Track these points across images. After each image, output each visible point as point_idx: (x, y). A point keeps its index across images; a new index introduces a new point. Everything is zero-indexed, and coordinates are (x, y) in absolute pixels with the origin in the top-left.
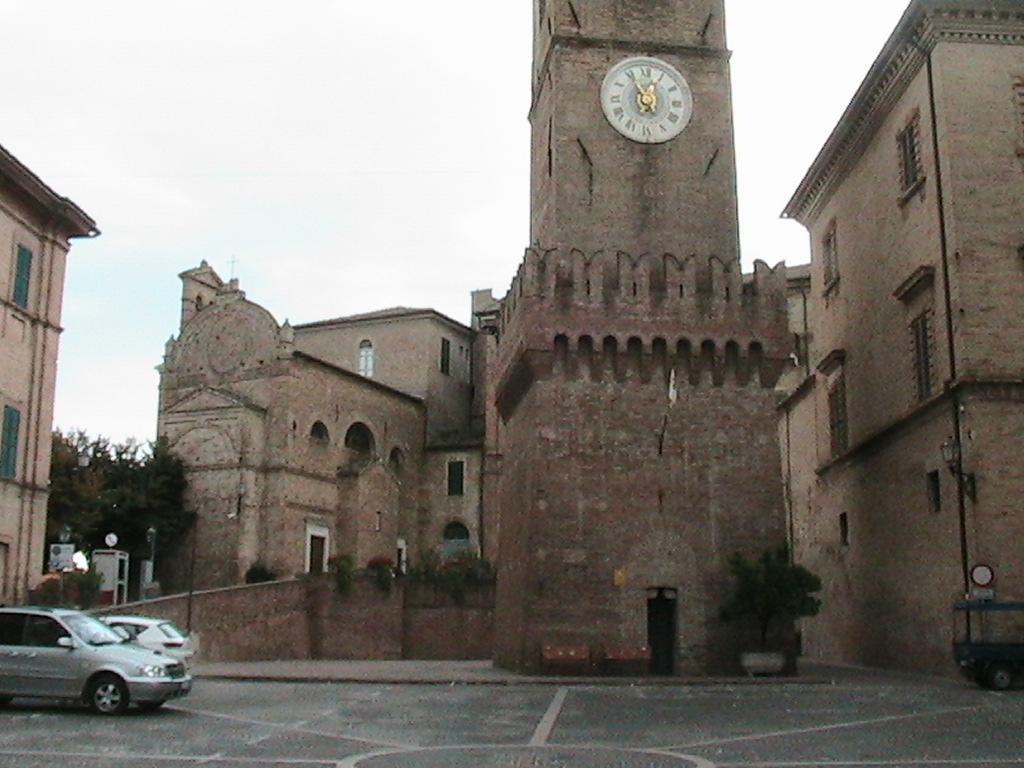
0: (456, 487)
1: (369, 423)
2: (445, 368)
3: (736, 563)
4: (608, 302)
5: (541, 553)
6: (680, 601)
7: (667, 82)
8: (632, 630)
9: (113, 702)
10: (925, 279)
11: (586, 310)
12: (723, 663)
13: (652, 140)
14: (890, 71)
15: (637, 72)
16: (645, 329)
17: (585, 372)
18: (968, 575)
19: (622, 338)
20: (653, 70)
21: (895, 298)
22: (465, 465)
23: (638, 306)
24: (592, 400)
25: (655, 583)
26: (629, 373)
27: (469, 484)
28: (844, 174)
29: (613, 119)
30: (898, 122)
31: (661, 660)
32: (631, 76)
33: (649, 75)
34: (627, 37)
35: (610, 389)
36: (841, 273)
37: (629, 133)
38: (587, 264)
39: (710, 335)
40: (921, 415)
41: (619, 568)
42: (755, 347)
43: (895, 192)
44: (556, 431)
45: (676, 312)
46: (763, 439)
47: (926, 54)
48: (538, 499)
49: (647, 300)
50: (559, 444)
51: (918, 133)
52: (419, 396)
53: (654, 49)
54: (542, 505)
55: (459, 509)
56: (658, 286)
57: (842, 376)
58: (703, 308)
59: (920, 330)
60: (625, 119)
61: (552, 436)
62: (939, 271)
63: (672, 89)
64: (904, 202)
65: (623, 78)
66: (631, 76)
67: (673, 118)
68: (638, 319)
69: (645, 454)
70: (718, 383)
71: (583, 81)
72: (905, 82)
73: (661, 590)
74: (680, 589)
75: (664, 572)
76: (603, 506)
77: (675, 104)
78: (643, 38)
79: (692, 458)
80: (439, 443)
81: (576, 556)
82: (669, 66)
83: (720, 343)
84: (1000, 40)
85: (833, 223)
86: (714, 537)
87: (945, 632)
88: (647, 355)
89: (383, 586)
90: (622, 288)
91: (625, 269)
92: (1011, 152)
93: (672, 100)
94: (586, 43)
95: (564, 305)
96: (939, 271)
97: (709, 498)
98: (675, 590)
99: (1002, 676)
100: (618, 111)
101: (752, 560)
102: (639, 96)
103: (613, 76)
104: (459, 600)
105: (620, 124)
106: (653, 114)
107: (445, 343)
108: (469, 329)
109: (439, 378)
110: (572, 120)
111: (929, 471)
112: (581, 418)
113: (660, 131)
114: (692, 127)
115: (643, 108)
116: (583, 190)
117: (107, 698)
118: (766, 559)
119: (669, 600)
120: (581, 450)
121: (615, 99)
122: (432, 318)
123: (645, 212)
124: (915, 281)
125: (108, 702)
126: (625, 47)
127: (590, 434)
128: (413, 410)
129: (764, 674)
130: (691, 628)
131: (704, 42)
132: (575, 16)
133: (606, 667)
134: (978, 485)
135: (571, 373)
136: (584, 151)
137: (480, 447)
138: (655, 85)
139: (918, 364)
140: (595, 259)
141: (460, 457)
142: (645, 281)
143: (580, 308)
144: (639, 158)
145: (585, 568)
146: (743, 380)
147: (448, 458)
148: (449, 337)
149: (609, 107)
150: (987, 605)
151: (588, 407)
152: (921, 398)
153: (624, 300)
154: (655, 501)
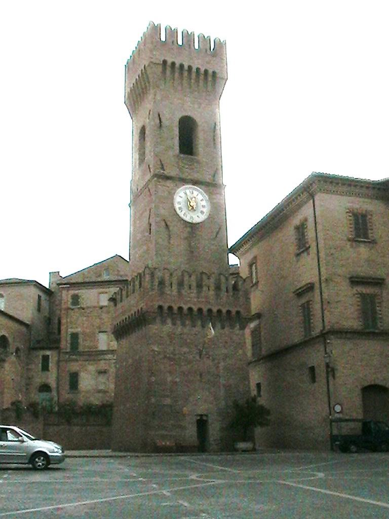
0: (45, 368)
1: (7, 335)
2: (39, 310)
3: (236, 405)
4: (179, 292)
5: (153, 400)
6: (210, 421)
7: (200, 197)
8: (191, 433)
9: (43, 464)
10: (310, 288)
11: (170, 295)
12: (228, 447)
13: (194, 222)
14: (293, 200)
15: (188, 191)
16: (195, 304)
17: (169, 321)
18: (331, 409)
19: (185, 307)
20: (194, 191)
21: (294, 294)
22: (50, 357)
23: (192, 294)
24: (172, 334)
25: (199, 413)
26: (187, 322)
27: (52, 365)
28: (262, 238)
29: (178, 211)
30: (296, 221)
31: (201, 447)
32: (186, 194)
33: (193, 193)
34: (183, 176)
35: (179, 330)
36: (260, 280)
37: (185, 218)
38: (171, 275)
39: (220, 307)
40: (305, 344)
41: (185, 406)
42: (238, 313)
43: (293, 249)
44: (158, 347)
45: (206, 297)
46: (240, 352)
47: (312, 196)
48: (150, 376)
49: (195, 291)
50: (159, 353)
51: (307, 227)
52: (28, 323)
53: (195, 183)
54: (153, 379)
55: (47, 378)
56: (199, 286)
57: (259, 324)
58: (218, 296)
59: (306, 309)
60: (183, 213)
61: (156, 349)
62: (317, 285)
63: (202, 200)
64: (298, 255)
65: (182, 194)
66: (186, 194)
67: (202, 212)
68: (191, 300)
69: (194, 357)
70: (223, 328)
71: (166, 194)
72: (300, 206)
73: (201, 415)
74: (209, 415)
75: (202, 409)
76: (178, 380)
77: (203, 206)
78: (189, 177)
79: (213, 360)
80: (37, 346)
81: (168, 401)
82: (201, 190)
83: (224, 311)
84: (342, 194)
85: (255, 258)
86: (222, 392)
87: (322, 433)
88: (195, 315)
89: (35, 415)
90: (185, 286)
91: (186, 278)
92: (345, 238)
93: (202, 204)
94: (168, 178)
95: (162, 293)
96: (317, 285)
97: (220, 377)
98: (206, 416)
99: (353, 448)
100: (180, 208)
101: (241, 402)
102: (189, 203)
103: (179, 193)
104: (69, 422)
105: (181, 215)
106: (195, 210)
107: (39, 297)
108: (47, 289)
109: (36, 313)
110: (162, 211)
111: (310, 366)
112: (168, 343)
113: (197, 218)
114: (210, 217)
115: (191, 208)
116: (166, 243)
117: (40, 463)
118: (247, 402)
119: (204, 420)
120: (168, 355)
121: (179, 203)
122: (35, 285)
123: (192, 252)
124: (305, 288)
125: (41, 464)
126: (184, 181)
127: (172, 349)
128: (24, 329)
129: (244, 451)
130: (215, 430)
131: (214, 181)
132: (162, 165)
133: (181, 449)
134: (336, 372)
135: (164, 322)
136: (167, 225)
137: (58, 348)
138: (195, 198)
139: (304, 322)
140: (175, 273)
141: (48, 353)
142: (194, 284)
143: (168, 295)
144: (189, 229)
145: (171, 406)
146: (232, 326)
147: (42, 353)
148: (41, 294)
149: (177, 206)
150: (341, 420)
151: (171, 336)
152: (305, 336)
153: (186, 292)
154: (198, 377)
